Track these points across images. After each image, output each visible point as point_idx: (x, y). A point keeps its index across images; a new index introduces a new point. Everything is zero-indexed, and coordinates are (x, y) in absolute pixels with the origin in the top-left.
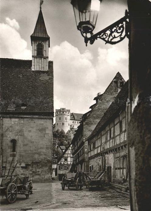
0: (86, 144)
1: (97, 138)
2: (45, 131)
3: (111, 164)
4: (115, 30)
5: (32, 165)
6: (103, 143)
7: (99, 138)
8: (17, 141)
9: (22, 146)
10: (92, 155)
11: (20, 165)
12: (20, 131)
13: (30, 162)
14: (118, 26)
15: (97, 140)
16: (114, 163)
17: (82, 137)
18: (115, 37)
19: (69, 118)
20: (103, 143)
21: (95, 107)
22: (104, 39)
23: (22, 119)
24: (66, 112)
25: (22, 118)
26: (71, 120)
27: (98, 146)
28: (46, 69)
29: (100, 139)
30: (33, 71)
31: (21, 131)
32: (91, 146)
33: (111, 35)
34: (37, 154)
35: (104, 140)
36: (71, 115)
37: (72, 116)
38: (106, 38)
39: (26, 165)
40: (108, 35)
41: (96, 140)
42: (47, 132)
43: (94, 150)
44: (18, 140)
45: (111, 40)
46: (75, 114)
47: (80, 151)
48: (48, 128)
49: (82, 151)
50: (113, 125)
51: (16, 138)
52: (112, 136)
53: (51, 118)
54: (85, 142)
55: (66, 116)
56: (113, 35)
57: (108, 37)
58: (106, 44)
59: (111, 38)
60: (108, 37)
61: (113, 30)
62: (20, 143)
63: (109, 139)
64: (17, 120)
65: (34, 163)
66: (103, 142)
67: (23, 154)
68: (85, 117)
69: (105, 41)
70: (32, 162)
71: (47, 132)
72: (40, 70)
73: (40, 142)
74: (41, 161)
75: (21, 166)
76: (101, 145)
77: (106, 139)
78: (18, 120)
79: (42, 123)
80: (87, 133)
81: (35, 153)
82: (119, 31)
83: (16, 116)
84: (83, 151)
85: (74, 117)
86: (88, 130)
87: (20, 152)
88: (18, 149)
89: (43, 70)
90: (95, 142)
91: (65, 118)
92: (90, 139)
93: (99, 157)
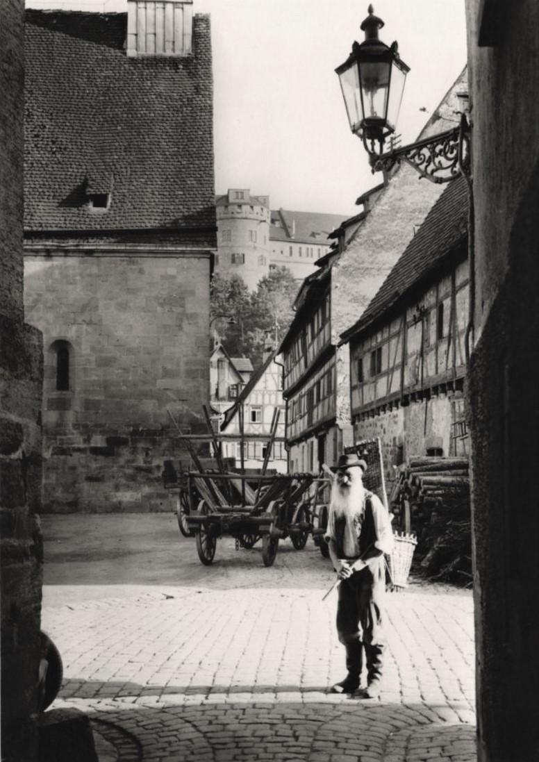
0: (344, 353)
1: (386, 335)
2: (183, 306)
3: (442, 441)
4: (441, 151)
5: (135, 442)
6: (412, 355)
7: (398, 334)
8: (74, 346)
9: (93, 366)
10: (366, 402)
11: (87, 440)
12: (84, 308)
13: (126, 429)
14: (448, 143)
15: (389, 340)
16: (453, 438)
17: (323, 325)
18: (440, 167)
19: (264, 230)
20: (412, 355)
21: (379, 199)
22: (417, 166)
23: (94, 260)
24: (252, 207)
25: (89, 253)
26: (272, 239)
27: (391, 365)
28: (184, 47)
29: (401, 337)
30: (132, 59)
31: (88, 307)
32: (364, 362)
33: (430, 161)
34: (153, 397)
35: (414, 345)
36: (273, 221)
37: (278, 224)
38: (421, 164)
39: (108, 440)
40: (427, 158)
41: (383, 342)
42: (191, 307)
43: (375, 382)
44: (79, 344)
45: (433, 171)
46: (289, 213)
47: (318, 383)
48: (192, 293)
49: (324, 383)
50: (450, 289)
51: (71, 334)
52: (446, 331)
53: (208, 252)
54: (340, 345)
55: (252, 226)
56: (437, 160)
57: (425, 164)
58: (420, 178)
59: (432, 167)
60: (425, 164)
61: (406, 494)
62: (83, 354)
63: (433, 339)
64: (72, 261)
65: (141, 434)
66: (410, 351)
67: (97, 398)
68: (342, 234)
69: (420, 170)
70: (131, 429)
71: (191, 307)
72: (160, 52)
73: (162, 348)
74: (168, 427)
75: (92, 445)
76: (404, 363)
77: (424, 340)
78: (77, 264)
79: (172, 271)
80: (346, 310)
81: (145, 395)
82: (449, 155)
83: (71, 244)
84: (329, 386)
85: (285, 227)
86: (350, 298)
87: (86, 391)
88: (79, 380)
89: (169, 53)
90: (380, 350)
91: (247, 234)
92: (356, 337)
93: (394, 408)
